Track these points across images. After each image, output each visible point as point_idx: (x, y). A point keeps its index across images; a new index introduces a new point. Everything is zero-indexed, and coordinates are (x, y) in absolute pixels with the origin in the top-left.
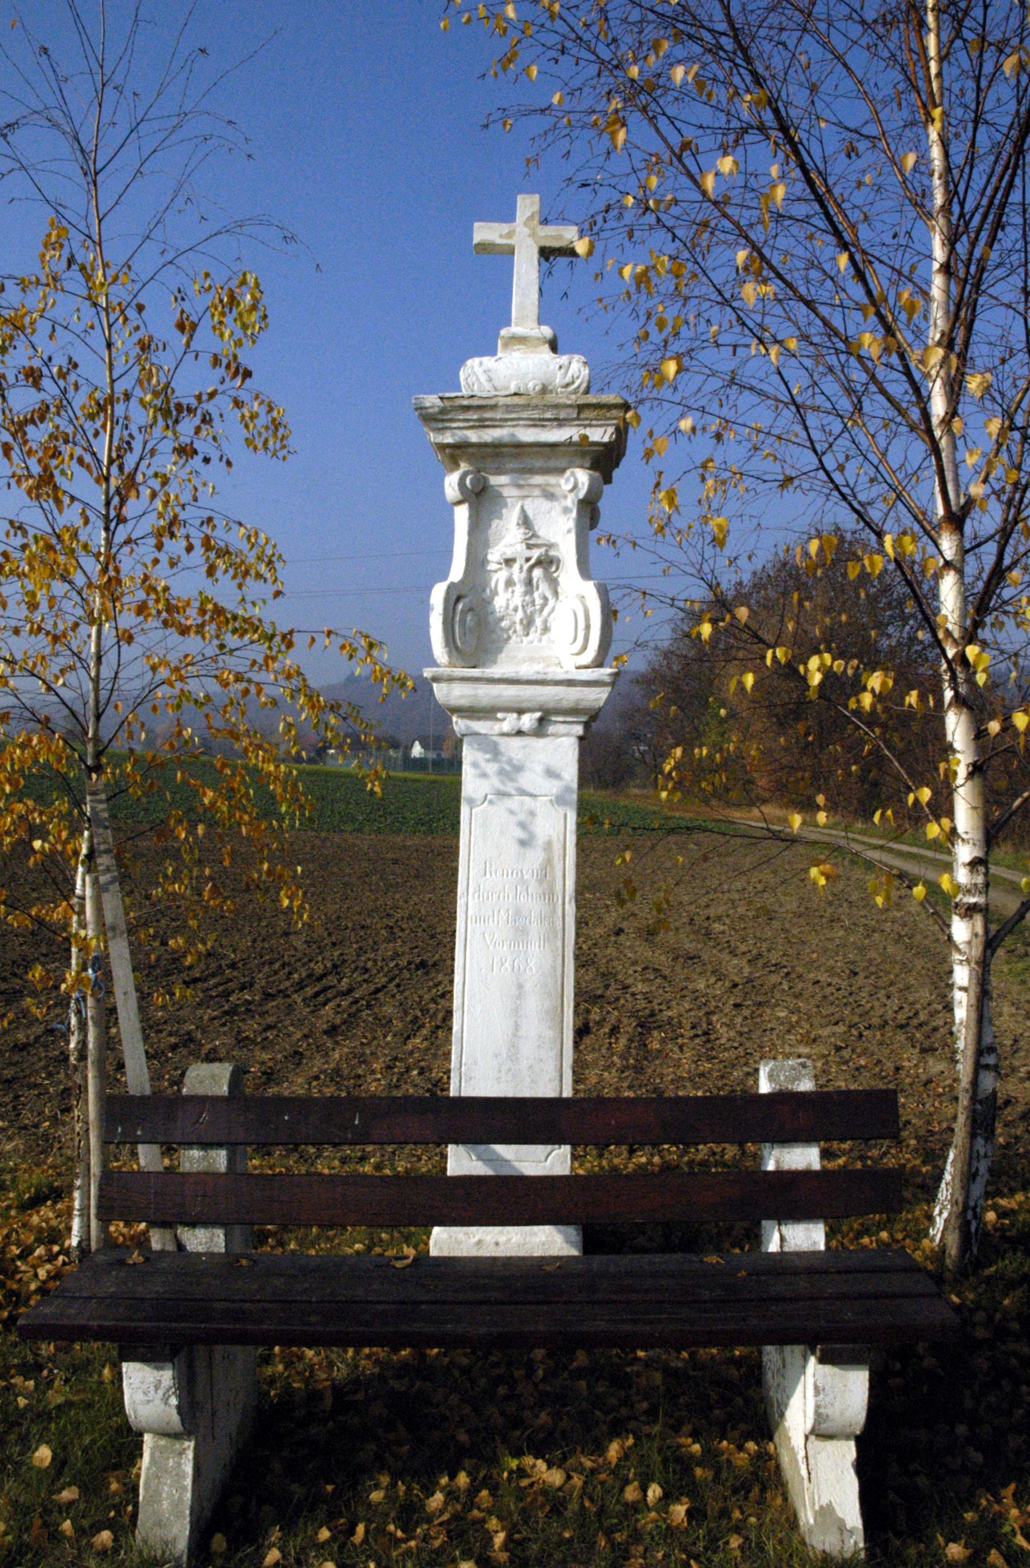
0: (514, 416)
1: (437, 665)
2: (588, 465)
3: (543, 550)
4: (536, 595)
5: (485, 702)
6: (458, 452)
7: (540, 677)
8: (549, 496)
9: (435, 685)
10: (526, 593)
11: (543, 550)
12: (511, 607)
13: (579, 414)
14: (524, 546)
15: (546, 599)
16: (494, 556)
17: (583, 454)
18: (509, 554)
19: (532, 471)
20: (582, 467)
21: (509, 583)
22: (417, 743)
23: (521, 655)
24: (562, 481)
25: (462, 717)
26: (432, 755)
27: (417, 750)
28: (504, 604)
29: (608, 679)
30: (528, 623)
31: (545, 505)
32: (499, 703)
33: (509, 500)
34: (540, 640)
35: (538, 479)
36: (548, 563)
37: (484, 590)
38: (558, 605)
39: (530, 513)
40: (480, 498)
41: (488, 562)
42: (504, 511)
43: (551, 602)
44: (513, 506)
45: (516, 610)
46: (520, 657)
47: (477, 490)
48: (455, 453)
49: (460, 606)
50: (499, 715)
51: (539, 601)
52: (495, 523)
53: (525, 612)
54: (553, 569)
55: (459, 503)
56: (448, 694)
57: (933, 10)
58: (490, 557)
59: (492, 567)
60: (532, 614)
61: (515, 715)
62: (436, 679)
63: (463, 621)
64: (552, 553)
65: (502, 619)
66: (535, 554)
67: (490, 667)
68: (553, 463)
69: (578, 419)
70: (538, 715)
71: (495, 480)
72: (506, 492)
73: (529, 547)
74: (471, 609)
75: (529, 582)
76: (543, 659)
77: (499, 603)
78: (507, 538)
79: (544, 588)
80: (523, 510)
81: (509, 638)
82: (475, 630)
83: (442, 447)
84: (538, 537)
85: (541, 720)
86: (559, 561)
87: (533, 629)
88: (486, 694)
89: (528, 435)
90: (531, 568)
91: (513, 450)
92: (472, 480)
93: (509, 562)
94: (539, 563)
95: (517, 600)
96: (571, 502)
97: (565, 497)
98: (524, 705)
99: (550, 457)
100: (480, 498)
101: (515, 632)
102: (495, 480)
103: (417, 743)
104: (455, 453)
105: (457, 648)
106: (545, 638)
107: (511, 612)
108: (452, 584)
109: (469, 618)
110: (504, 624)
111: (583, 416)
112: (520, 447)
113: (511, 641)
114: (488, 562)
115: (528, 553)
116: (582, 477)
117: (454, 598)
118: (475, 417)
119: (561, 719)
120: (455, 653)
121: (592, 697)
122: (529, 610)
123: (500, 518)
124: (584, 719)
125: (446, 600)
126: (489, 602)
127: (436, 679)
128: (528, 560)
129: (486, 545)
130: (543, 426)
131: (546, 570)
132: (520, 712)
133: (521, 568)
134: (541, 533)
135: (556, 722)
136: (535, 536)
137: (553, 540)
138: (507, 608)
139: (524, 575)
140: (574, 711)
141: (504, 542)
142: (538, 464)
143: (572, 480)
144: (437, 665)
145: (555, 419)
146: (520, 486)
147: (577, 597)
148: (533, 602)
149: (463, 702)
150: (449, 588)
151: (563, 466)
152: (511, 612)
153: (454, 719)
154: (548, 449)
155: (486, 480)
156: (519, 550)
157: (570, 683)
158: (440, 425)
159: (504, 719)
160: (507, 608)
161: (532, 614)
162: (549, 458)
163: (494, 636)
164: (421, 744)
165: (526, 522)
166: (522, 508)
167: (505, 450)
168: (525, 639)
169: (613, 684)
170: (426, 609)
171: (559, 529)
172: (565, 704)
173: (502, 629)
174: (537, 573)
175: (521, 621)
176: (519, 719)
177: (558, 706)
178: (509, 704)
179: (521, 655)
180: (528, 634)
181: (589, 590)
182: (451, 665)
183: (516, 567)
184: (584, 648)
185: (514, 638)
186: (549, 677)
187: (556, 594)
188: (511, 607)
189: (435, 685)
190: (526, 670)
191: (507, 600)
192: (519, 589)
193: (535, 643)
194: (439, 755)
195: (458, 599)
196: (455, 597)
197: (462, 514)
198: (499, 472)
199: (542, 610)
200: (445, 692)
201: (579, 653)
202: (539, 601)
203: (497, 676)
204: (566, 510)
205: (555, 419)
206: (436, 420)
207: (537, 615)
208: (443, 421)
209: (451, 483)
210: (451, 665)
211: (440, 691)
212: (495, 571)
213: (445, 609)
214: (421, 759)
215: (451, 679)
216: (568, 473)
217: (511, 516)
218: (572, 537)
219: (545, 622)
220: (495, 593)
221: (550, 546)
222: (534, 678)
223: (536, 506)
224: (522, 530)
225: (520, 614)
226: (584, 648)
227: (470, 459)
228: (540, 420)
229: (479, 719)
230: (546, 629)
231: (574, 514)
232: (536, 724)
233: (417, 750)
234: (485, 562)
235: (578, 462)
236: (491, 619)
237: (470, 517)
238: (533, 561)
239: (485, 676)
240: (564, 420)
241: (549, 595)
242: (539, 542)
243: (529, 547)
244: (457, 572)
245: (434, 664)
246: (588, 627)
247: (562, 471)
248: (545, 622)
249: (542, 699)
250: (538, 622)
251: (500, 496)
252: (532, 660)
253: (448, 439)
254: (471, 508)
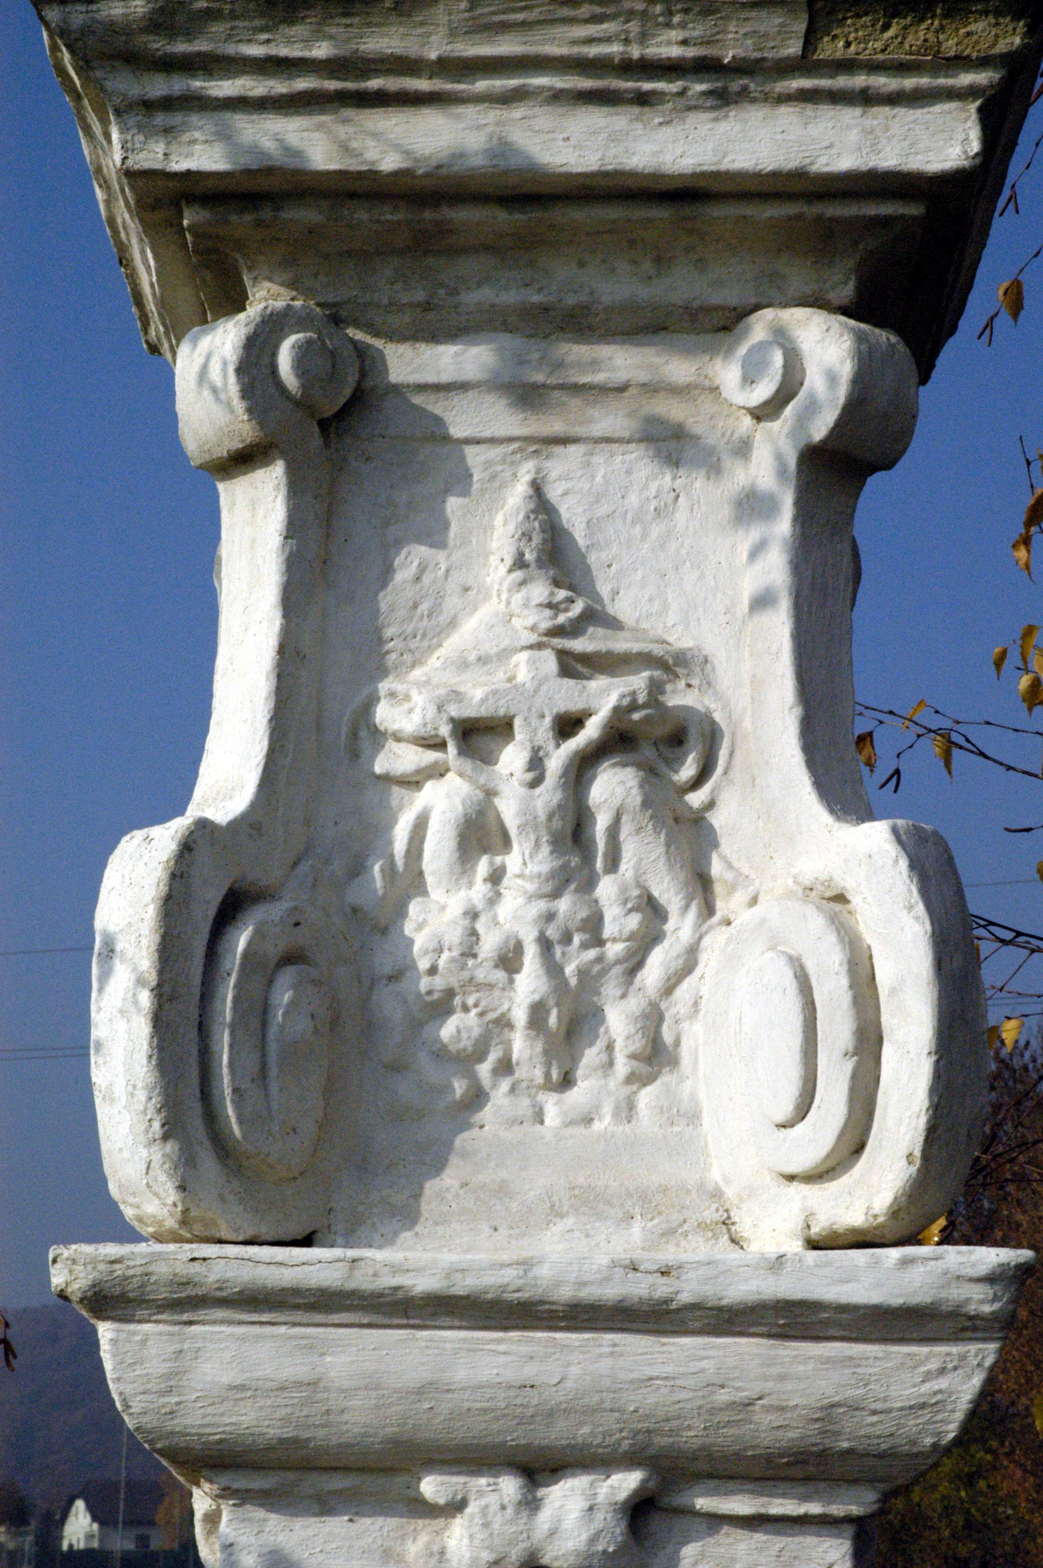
0: (506, 47)
1: (128, 1234)
2: (846, 292)
3: (638, 682)
4: (606, 889)
5: (358, 1418)
6: (241, 222)
7: (640, 1288)
8: (670, 443)
9: (105, 1331)
10: (559, 883)
11: (638, 682)
12: (489, 944)
13: (810, 41)
14: (549, 662)
15: (652, 909)
16: (406, 708)
17: (822, 241)
18: (477, 698)
19: (581, 323)
20: (817, 302)
21: (480, 834)
22: (80, 1505)
23: (536, 1183)
24: (728, 374)
25: (243, 1497)
26: (122, 1543)
27: (79, 1528)
28: (454, 936)
29: (982, 1301)
30: (569, 1027)
31: (639, 475)
32: (434, 1420)
33: (474, 456)
34: (627, 1110)
35: (621, 361)
36: (662, 740)
37: (358, 869)
38: (715, 941)
39: (573, 515)
40: (336, 436)
41: (378, 737)
42: (453, 503)
43: (680, 927)
44: (497, 483)
45: (509, 960)
46: (519, 1197)
47: (329, 409)
48: (218, 231)
49: (242, 939)
50: (432, 1487)
51: (619, 923)
52: (410, 559)
53: (553, 969)
54: (688, 771)
55: (243, 460)
56: (172, 1382)
57: (521, 828)
58: (385, 715)
59: (399, 759)
60: (590, 978)
61: (510, 1486)
62: (110, 1301)
63: (255, 1012)
64: (680, 697)
65: (442, 1006)
66: (604, 698)
67: (388, 1241)
68: (683, 286)
69: (804, 64)
70: (626, 1482)
71: (407, 363)
72: (462, 419)
73: (572, 666)
74: (291, 958)
75: (572, 830)
76: (647, 1201)
77: (432, 924)
78: (470, 624)
79: (645, 857)
80: (540, 503)
81: (477, 1098)
82: (310, 1053)
83: (164, 198)
84: (613, 624)
85: (640, 1511)
86: (712, 737)
87: (591, 1056)
88: (364, 1375)
89: (573, 142)
90: (583, 767)
91: (501, 217)
92: (302, 358)
93: (478, 736)
94: (619, 740)
95: (516, 913)
96: (767, 461)
97: (743, 449)
98: (557, 1433)
99: (672, 253)
100: (336, 436)
101: (505, 1067)
102: (407, 363)
103: (80, 1505)
104: (218, 231)
105: (222, 1146)
106: (646, 1097)
107: (485, 972)
108: (199, 840)
109: (283, 996)
110: (455, 1029)
111: (831, 49)
112: (531, 203)
113: (487, 1114)
114: (378, 737)
115: (568, 695)
116: (826, 348)
117: (212, 897)
118: (321, 51)
119: (741, 1505)
120: (209, 1164)
121: (905, 1390)
122: (575, 961)
123: (435, 534)
124: (853, 1505)
125: (174, 904)
126: (380, 923)
127: (110, 1301)
128: (567, 725)
129: (371, 661)
130: (643, 100)
131: (652, 775)
132: (538, 1468)
133: (536, 763)
134: (622, 608)
135: (717, 1520)
136: (594, 617)
137: (681, 640)
138: (469, 953)
139: (548, 795)
140: (804, 1465)
141: (453, 644)
142: (617, 286)
143: (778, 358)
144: (128, 1234)
145: (704, 67)
146: (527, 396)
147: (811, 906)
148: (593, 927)
149: (250, 1420)
150: (187, 847)
151: (730, 296)
152: (485, 972)
153: (201, 1502)
154: (661, 213)
155: (367, 362)
156: (528, 679)
157: (794, 1320)
158: (158, 86)
159: (456, 1507)
160: (469, 953)
161: (590, 978)
162: (662, 262)
163: (405, 1089)
164: (90, 1508)
165: (553, 552)
166: (537, 488)
167: (463, 215)
168: (553, 1106)
169: (1004, 1326)
170: (72, 953)
171: (715, 589)
172: (766, 1430)
173: (441, 1054)
174: (612, 787)
175: (537, 1013)
176: (531, 1504)
177: (728, 1438)
178: (475, 1430)
179: (536, 1183)
180: (567, 1082)
181: (868, 857)
182: (190, 1228)
183: (512, 759)
184: (853, 1143)
185: (500, 1095)
186: (688, 1290)
187: (701, 886)
188: (489, 944)
189: (105, 1331)
190: (569, 1257)
191: (462, 912)
192: (526, 862)
193: (603, 1124)
194: (143, 1541)
195: (232, 907)
196: (212, 895)
197: (254, 523)
198: (433, 327)
199: (634, 962)
200: (156, 1366)
201: (822, 1173)
202: (619, 923)
203: (422, 1284)
204: (751, 506)
205: (704, 67)
206: (136, 61)
207: (610, 989)
208: (170, 65)
209: (205, 373)
210: (190, 1228)
211: (130, 1359)
212: (413, 782)
213: (168, 950)
214: (88, 1553)
215: (187, 1302)
216: (760, 326)
217: (490, 528)
218: (779, 627)
219: (652, 1019)
220: (411, 882)
221: (669, 665)
222: (611, 1292)
223: (601, 486)
224: (539, 591)
225: (529, 983)
226: (853, 1143)
227: (294, 258)
228: (628, 68)
229: (324, 1505)
230: (656, 1055)
231: (784, 525)
232: (612, 1533)
233: (79, 1528)
234: (363, 734)
235: (799, 277)
236: (389, 1006)
237: (293, 529)
238: (591, 731)
239: (363, 1281)
240: (742, 68)
241: (667, 890)
242: (621, 644)
243: (572, 666)
244: (229, 775)
245: (109, 1223)
246: (869, 1042)
247: (723, 324)
248: (652, 1019)
249: (649, 1400)
250: (619, 1020)
251: (436, 434)
252: (589, 1202)
253: (201, 153)
254: (296, 488)
